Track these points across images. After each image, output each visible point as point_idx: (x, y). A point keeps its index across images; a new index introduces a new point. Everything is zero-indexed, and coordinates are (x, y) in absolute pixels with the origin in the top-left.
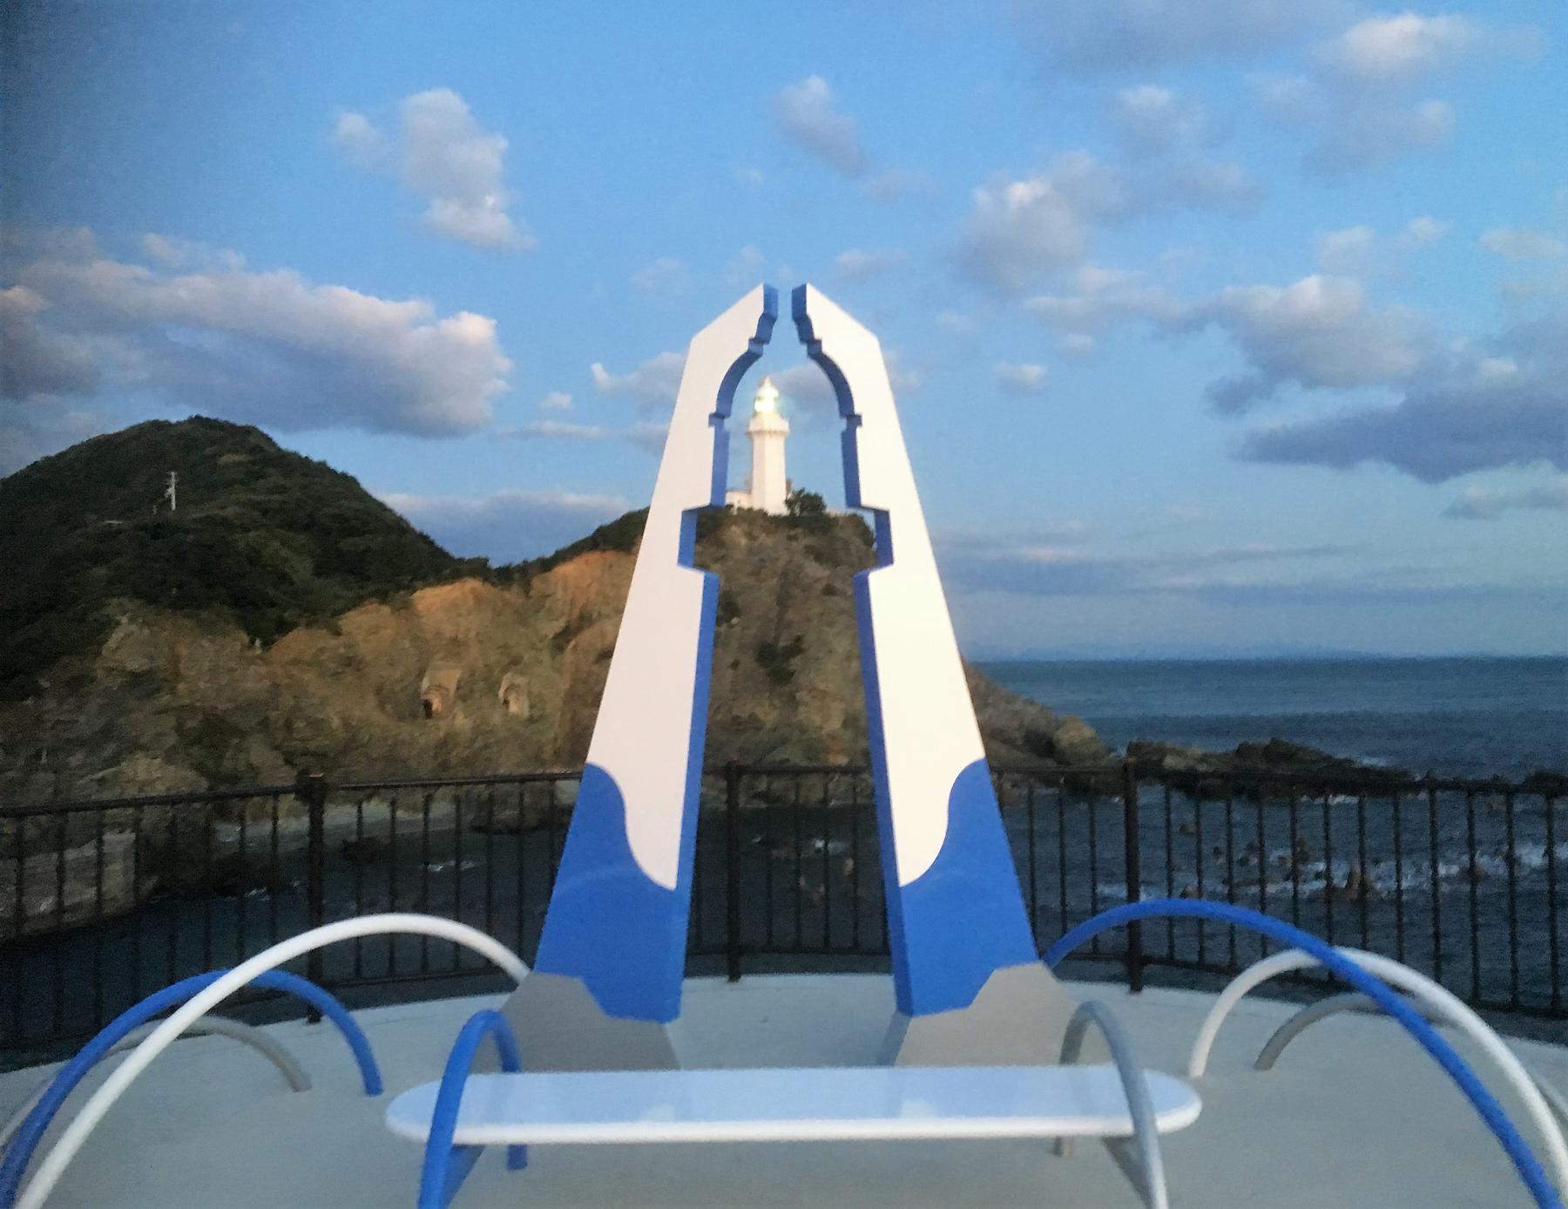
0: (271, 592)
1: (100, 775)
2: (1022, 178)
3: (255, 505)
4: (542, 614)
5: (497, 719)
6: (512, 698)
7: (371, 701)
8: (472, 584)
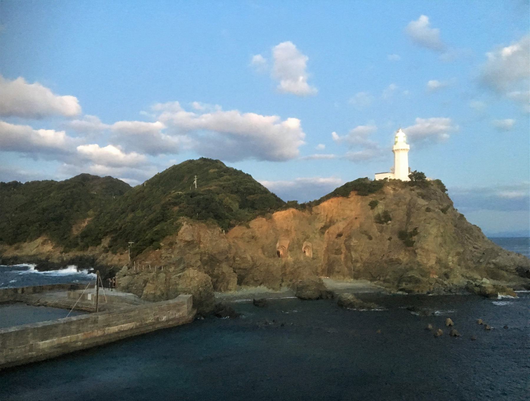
0: (227, 214)
1: (179, 275)
2: (507, 46)
3: (221, 186)
4: (316, 220)
5: (302, 258)
6: (306, 251)
7: (260, 251)
8: (292, 210)
